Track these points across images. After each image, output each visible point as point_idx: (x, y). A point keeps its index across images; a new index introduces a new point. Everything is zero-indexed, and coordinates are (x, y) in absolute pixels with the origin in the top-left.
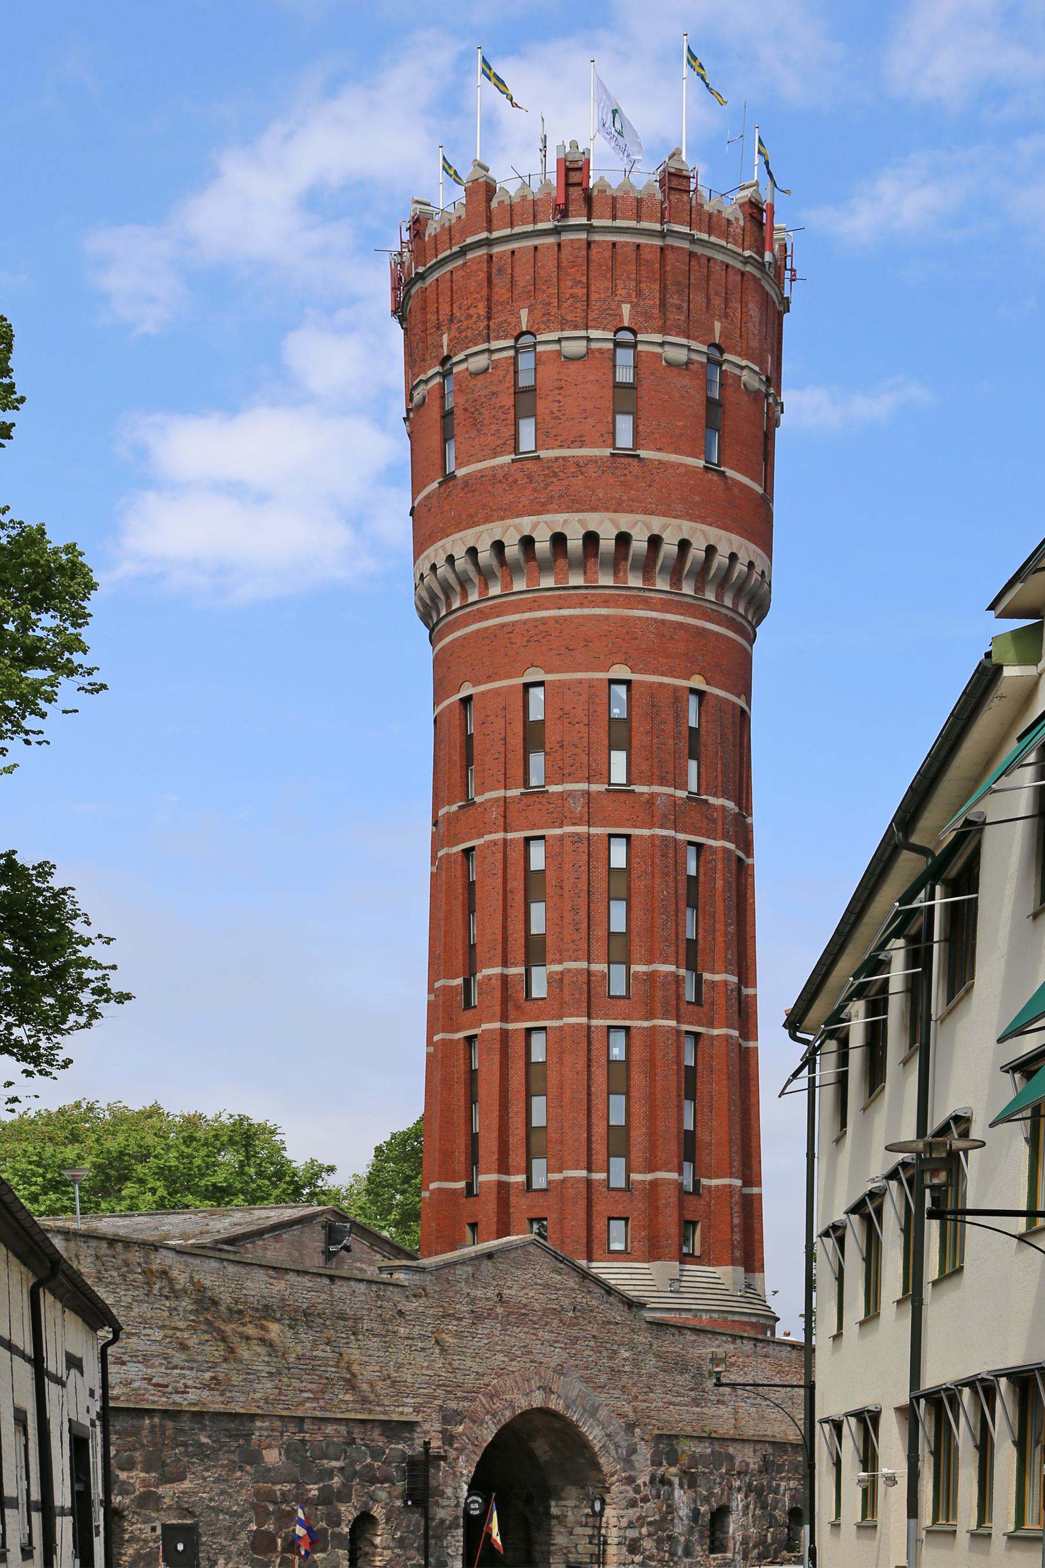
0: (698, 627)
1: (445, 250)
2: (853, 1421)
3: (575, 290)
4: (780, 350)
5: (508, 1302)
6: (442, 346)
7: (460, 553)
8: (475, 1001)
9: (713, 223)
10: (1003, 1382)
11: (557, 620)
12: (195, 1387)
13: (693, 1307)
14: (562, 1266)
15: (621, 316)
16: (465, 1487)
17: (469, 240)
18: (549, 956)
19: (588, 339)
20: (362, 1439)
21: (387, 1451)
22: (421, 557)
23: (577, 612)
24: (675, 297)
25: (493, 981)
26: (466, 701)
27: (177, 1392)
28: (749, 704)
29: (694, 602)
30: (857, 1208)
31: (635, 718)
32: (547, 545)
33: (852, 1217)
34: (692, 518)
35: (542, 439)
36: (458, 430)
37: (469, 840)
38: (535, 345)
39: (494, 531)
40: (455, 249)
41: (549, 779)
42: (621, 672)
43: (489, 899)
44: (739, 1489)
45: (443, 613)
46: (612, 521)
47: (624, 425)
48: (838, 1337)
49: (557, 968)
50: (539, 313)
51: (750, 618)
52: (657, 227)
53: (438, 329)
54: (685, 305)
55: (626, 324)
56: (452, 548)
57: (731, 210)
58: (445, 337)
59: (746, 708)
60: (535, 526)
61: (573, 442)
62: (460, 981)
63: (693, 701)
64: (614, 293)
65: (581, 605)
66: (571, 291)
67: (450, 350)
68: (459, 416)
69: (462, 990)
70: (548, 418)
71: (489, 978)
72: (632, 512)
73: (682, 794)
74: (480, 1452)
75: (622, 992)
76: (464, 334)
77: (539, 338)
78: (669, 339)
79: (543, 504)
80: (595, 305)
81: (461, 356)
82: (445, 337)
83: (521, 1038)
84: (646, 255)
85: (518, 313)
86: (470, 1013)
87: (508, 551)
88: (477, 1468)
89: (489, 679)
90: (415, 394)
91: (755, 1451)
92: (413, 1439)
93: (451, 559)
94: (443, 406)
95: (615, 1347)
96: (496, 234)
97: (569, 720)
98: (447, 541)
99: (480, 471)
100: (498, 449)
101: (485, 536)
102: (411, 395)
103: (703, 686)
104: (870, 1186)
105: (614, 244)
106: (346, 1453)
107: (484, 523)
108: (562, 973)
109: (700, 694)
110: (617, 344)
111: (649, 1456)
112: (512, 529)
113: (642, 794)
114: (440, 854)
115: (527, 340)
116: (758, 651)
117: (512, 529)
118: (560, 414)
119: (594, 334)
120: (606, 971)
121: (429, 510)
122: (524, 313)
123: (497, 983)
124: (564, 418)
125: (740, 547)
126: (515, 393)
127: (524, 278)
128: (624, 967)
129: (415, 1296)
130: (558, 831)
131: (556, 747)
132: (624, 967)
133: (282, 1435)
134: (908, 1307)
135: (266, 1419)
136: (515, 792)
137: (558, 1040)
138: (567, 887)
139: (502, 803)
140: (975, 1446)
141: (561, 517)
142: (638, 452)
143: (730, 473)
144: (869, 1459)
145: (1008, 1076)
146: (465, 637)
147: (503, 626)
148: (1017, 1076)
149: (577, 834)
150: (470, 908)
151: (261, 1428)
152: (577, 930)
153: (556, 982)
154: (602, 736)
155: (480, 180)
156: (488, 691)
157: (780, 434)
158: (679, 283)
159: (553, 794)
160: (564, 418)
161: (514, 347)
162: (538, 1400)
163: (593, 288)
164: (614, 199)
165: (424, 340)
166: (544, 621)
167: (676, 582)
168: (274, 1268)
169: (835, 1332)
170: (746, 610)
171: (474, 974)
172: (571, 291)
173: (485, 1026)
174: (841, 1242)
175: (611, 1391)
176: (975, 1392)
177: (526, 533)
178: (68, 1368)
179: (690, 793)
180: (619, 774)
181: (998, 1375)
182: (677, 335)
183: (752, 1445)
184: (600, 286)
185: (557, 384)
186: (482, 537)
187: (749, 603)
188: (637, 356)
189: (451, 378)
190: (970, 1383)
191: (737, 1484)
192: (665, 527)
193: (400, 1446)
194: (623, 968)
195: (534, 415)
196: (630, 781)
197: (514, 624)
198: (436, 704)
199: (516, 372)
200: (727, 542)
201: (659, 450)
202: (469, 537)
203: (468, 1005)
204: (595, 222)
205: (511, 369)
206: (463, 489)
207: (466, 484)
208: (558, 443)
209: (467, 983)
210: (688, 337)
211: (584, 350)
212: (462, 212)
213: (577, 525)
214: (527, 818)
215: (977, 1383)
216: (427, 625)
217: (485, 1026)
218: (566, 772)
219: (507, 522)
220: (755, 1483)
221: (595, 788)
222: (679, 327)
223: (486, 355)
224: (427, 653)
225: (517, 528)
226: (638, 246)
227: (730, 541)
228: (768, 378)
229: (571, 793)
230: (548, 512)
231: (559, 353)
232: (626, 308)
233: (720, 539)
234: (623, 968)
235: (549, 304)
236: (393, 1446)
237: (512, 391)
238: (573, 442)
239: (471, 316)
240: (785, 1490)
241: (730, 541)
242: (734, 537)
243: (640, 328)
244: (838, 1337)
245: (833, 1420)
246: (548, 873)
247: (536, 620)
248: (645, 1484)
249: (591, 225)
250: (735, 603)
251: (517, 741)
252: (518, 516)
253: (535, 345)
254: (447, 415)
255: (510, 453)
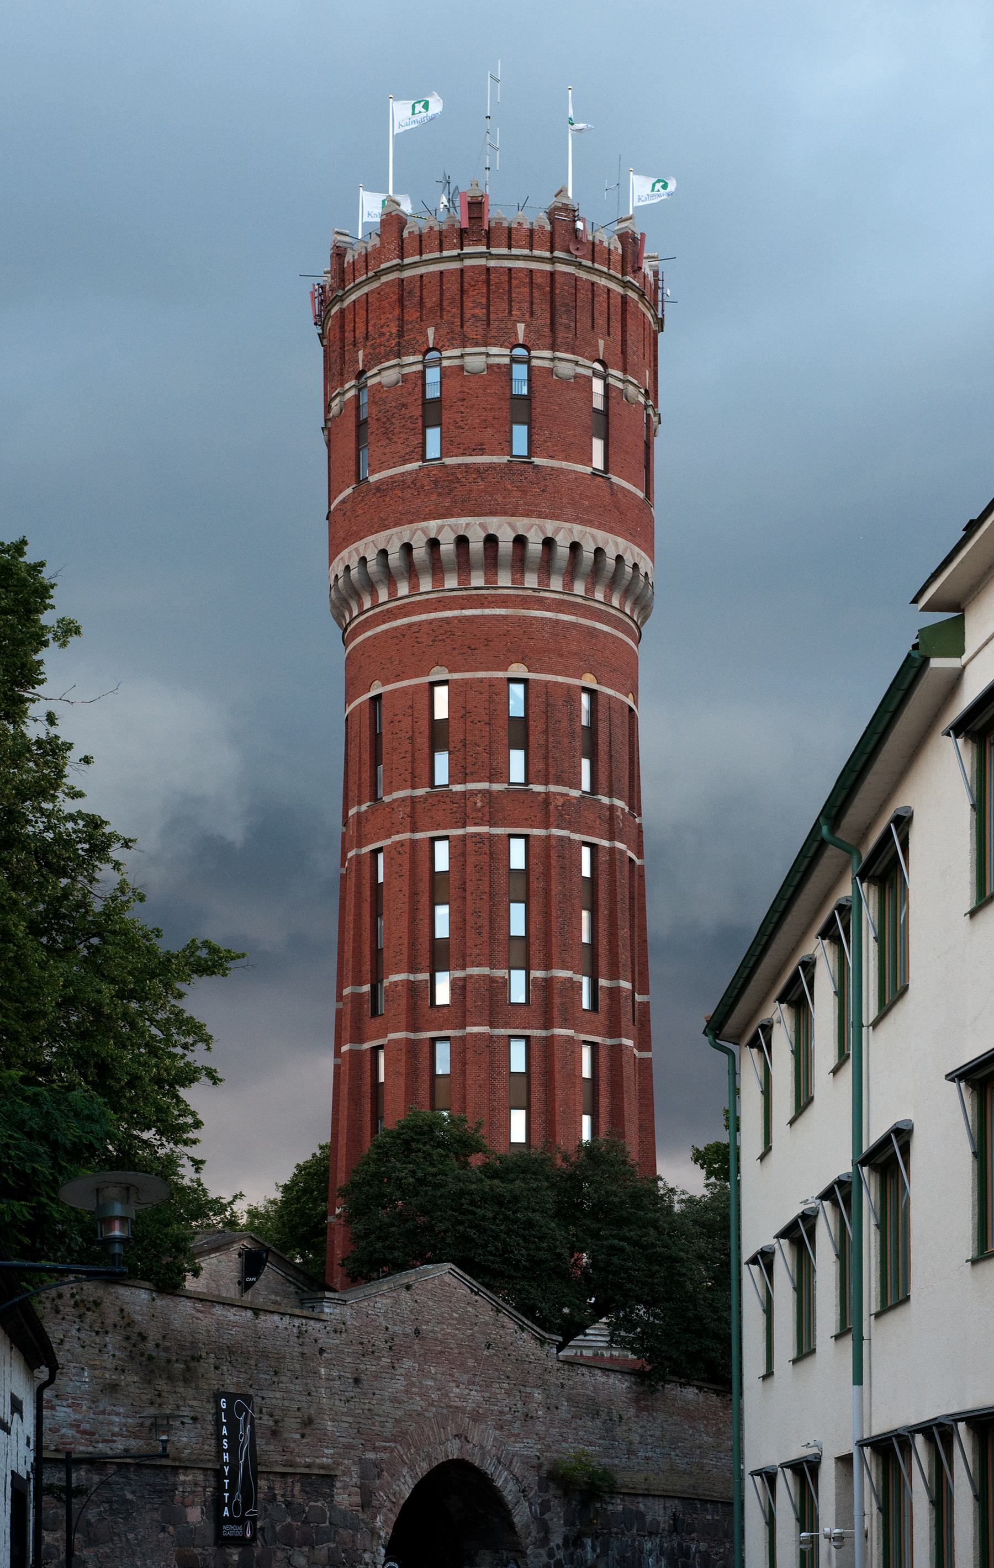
0: (588, 627)
1: (362, 275)
2: (788, 1472)
3: (477, 311)
4: (656, 366)
5: (424, 1338)
6: (357, 362)
7: (371, 555)
8: (382, 1009)
9: (594, 250)
10: (962, 1426)
11: (461, 619)
12: (122, 1436)
13: (595, 1344)
14: (477, 1298)
15: (516, 334)
16: (383, 1551)
17: (383, 266)
18: (453, 962)
19: (488, 355)
20: (282, 1496)
21: (307, 1509)
22: (337, 559)
23: (424, 617)
24: (564, 317)
25: (400, 988)
26: (378, 698)
27: (104, 1441)
28: (636, 702)
29: (584, 602)
30: (789, 1232)
31: (531, 715)
32: (452, 547)
33: (782, 1241)
34: (582, 522)
35: (447, 448)
36: (371, 438)
37: (378, 840)
38: (440, 359)
39: (404, 533)
40: (371, 274)
41: (453, 779)
42: (518, 670)
43: (396, 904)
44: (651, 1551)
45: (355, 613)
46: (510, 524)
47: (520, 434)
48: (769, 1374)
49: (459, 974)
50: (443, 332)
51: (635, 619)
52: (547, 254)
53: (354, 346)
54: (572, 324)
55: (521, 342)
56: (365, 550)
57: (608, 239)
58: (361, 353)
59: (634, 707)
60: (440, 529)
61: (474, 450)
62: (366, 988)
63: (585, 699)
64: (510, 313)
65: (482, 606)
66: (472, 312)
67: (365, 365)
68: (373, 424)
69: (368, 998)
70: (451, 427)
71: (396, 984)
72: (527, 515)
73: (575, 793)
74: (397, 1510)
75: (522, 999)
76: (377, 350)
77: (533, 353)
78: (559, 354)
79: (448, 508)
80: (494, 324)
81: (375, 371)
82: (361, 353)
83: (426, 1049)
84: (538, 280)
85: (426, 331)
86: (378, 1021)
87: (416, 553)
88: (394, 1529)
89: (398, 678)
90: (333, 404)
91: (665, 1508)
92: (333, 1496)
93: (363, 560)
94: (358, 416)
95: (528, 1390)
96: (407, 261)
97: (470, 719)
98: (360, 545)
99: (391, 477)
100: (407, 457)
101: (395, 538)
102: (329, 406)
103: (594, 686)
104: (802, 1208)
105: (510, 269)
106: (266, 1511)
107: (395, 526)
108: (465, 979)
109: (592, 693)
110: (514, 360)
111: (562, 1514)
112: (419, 532)
113: (539, 793)
114: (350, 855)
115: (434, 354)
116: (644, 652)
117: (419, 532)
118: (462, 424)
119: (493, 350)
120: (507, 977)
121: (344, 514)
122: (431, 332)
123: (402, 990)
124: (466, 427)
125: (625, 550)
126: (423, 404)
127: (431, 300)
128: (523, 972)
129: (335, 1331)
130: (460, 832)
131: (459, 745)
132: (523, 972)
133: (204, 1490)
134: (848, 1342)
135: (189, 1472)
136: (421, 792)
137: (460, 1050)
138: (470, 887)
139: (408, 802)
140: (931, 1502)
141: (463, 521)
142: (533, 459)
143: (615, 479)
144: (807, 1516)
145: (954, 1085)
146: (375, 637)
147: (410, 626)
148: (962, 1084)
149: (479, 834)
150: (376, 913)
151: (184, 1482)
152: (480, 933)
153: (458, 988)
154: (503, 735)
155: (393, 213)
156: (396, 690)
157: (659, 444)
158: (567, 305)
159: (457, 793)
160: (466, 427)
161: (422, 362)
162: (453, 1450)
163: (492, 308)
164: (510, 230)
165: (342, 357)
166: (447, 620)
167: (569, 584)
168: (201, 1300)
169: (763, 1371)
170: (632, 610)
171: (381, 982)
172: (472, 312)
173: (392, 1036)
174: (769, 1269)
175: (525, 1440)
176: (929, 1438)
177: (432, 536)
178: (12, 1414)
179: (584, 792)
180: (517, 773)
181: (957, 1418)
182: (566, 352)
183: (662, 1501)
184: (500, 305)
185: (460, 396)
186: (392, 539)
187: (635, 603)
188: (530, 369)
189: (366, 391)
190: (926, 1429)
191: (648, 1546)
192: (557, 530)
193: (319, 1504)
194: (522, 973)
195: (439, 424)
196: (527, 782)
197: (420, 623)
198: (348, 702)
199: (424, 385)
200: (615, 545)
201: (551, 457)
202: (379, 539)
203: (375, 1013)
204: (494, 251)
205: (419, 382)
206: (374, 494)
207: (378, 489)
208: (461, 451)
209: (374, 989)
210: (574, 353)
211: (483, 366)
212: (376, 241)
213: (479, 529)
214: (432, 818)
215: (934, 1429)
216: (340, 625)
217: (392, 1036)
218: (468, 771)
219: (415, 525)
220: (665, 1545)
221: (497, 787)
222: (568, 344)
223: (397, 369)
224: (340, 654)
225: (424, 531)
226: (531, 271)
227: (616, 544)
228: (646, 391)
229: (474, 793)
230: (452, 516)
231: (462, 368)
232: (521, 327)
233: (607, 542)
234: (522, 973)
235: (453, 323)
236: (312, 1503)
237: (420, 402)
238: (474, 450)
239: (384, 334)
240: (696, 1552)
241: (616, 544)
242: (620, 540)
243: (533, 345)
244: (769, 1374)
245: (766, 1473)
246: (451, 875)
247: (442, 620)
248: (558, 1546)
249: (490, 253)
250: (622, 604)
251: (423, 741)
252: (425, 519)
253: (440, 359)
254: (361, 425)
255: (418, 460)
